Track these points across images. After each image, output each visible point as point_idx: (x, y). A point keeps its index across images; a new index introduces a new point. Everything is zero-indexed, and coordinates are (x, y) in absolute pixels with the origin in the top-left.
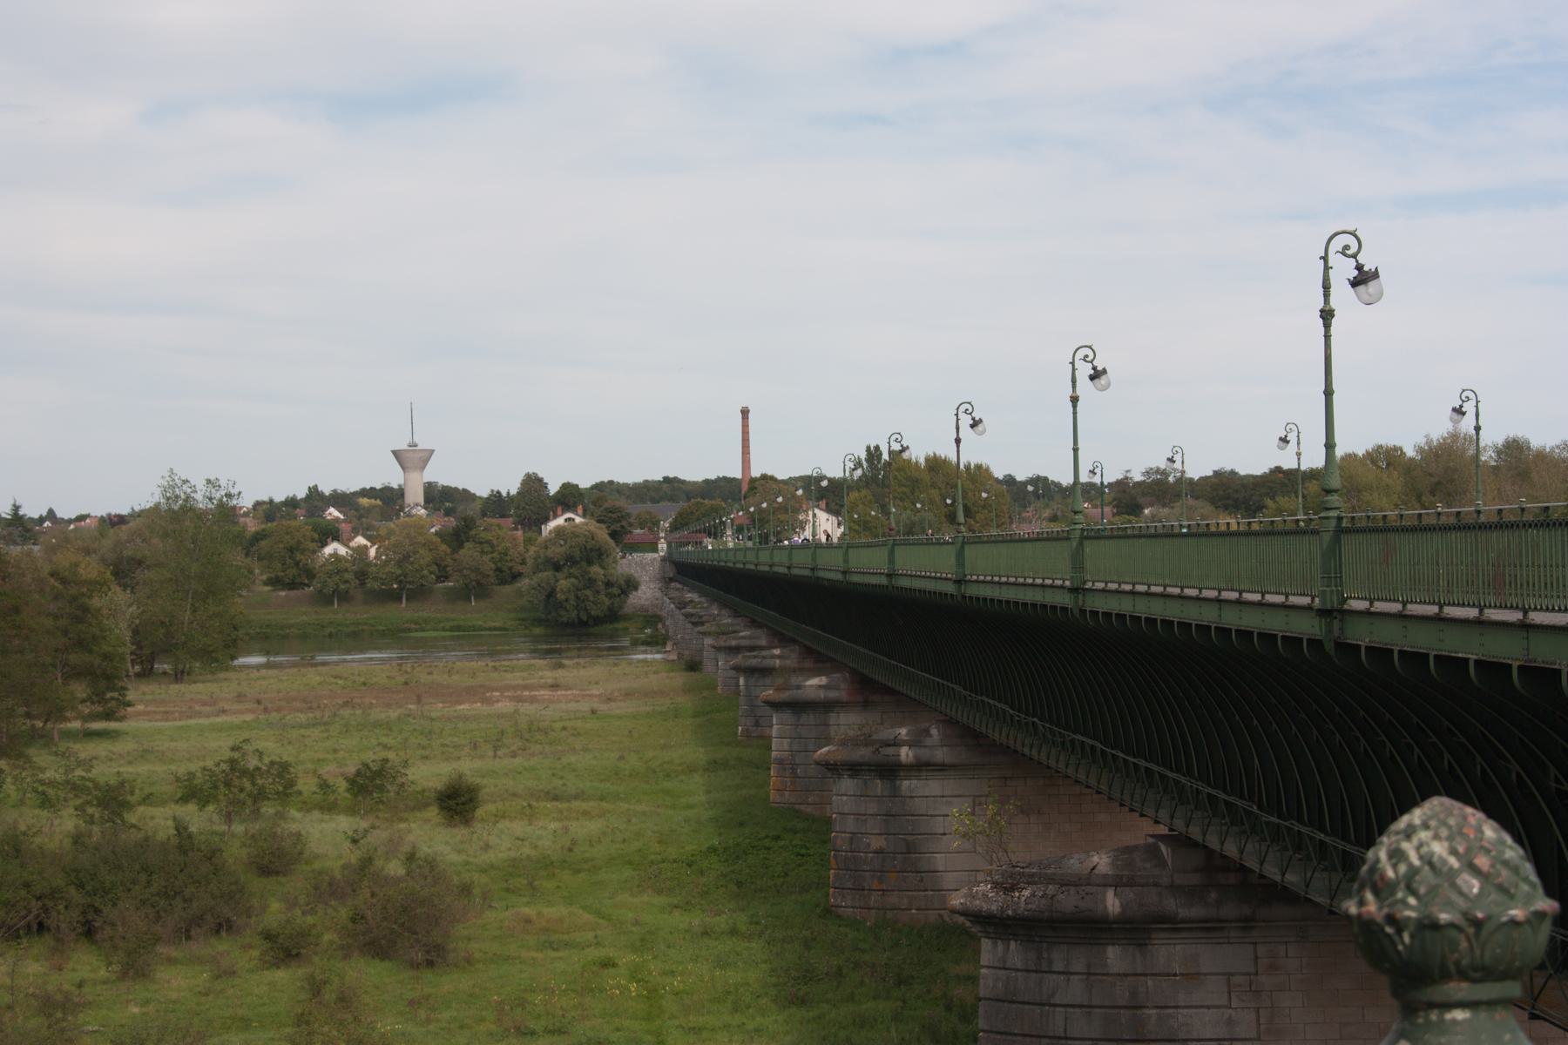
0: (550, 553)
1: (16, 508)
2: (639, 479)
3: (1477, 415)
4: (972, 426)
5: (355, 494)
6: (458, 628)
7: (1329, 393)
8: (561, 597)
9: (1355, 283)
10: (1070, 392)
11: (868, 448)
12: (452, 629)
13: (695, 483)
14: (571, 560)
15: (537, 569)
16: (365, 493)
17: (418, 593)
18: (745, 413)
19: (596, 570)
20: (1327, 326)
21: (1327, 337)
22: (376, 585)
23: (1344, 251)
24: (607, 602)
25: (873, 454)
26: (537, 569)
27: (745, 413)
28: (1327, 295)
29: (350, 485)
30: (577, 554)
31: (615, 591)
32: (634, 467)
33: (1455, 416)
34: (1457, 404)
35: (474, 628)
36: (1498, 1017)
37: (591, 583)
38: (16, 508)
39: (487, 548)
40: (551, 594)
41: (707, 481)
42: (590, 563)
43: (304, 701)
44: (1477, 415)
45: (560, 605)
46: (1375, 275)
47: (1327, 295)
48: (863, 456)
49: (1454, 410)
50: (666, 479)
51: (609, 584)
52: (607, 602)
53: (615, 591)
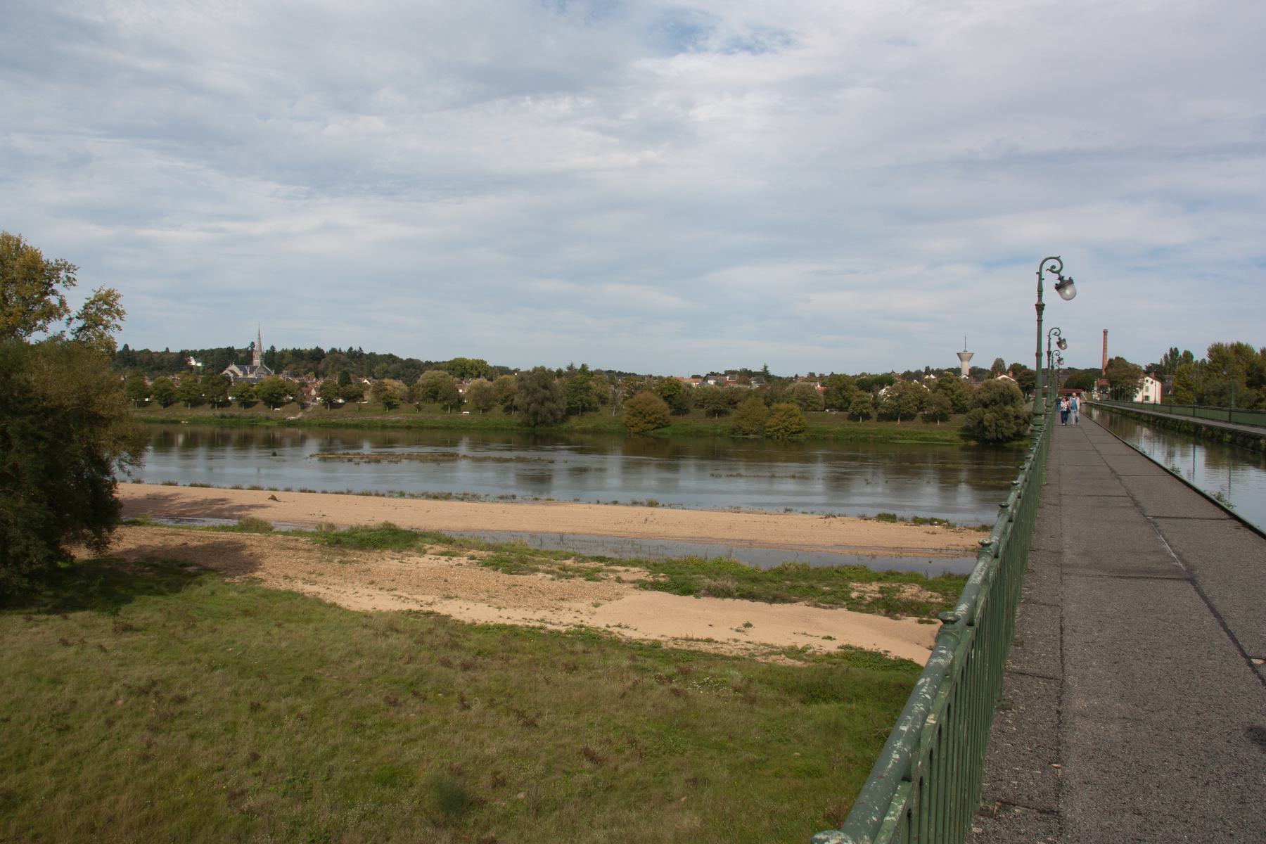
0: (981, 396)
4: (1058, 287)
6: (924, 439)
8: (986, 423)
9: (1058, 287)
10: (1036, 301)
12: (921, 439)
14: (994, 402)
15: (974, 406)
16: (949, 370)
17: (908, 417)
18: (1105, 332)
19: (1009, 408)
21: (1040, 321)
22: (884, 411)
23: (1052, 269)
24: (1015, 428)
25: (1174, 352)
26: (974, 406)
27: (1105, 332)
28: (1040, 296)
30: (998, 398)
31: (1021, 421)
32: (877, 369)
35: (934, 439)
37: (1006, 416)
39: (949, 392)
40: (981, 422)
41: (147, 352)
42: (1006, 404)
45: (985, 428)
46: (1071, 281)
47: (1040, 296)
51: (1017, 417)
52: (1015, 428)
53: (1021, 421)
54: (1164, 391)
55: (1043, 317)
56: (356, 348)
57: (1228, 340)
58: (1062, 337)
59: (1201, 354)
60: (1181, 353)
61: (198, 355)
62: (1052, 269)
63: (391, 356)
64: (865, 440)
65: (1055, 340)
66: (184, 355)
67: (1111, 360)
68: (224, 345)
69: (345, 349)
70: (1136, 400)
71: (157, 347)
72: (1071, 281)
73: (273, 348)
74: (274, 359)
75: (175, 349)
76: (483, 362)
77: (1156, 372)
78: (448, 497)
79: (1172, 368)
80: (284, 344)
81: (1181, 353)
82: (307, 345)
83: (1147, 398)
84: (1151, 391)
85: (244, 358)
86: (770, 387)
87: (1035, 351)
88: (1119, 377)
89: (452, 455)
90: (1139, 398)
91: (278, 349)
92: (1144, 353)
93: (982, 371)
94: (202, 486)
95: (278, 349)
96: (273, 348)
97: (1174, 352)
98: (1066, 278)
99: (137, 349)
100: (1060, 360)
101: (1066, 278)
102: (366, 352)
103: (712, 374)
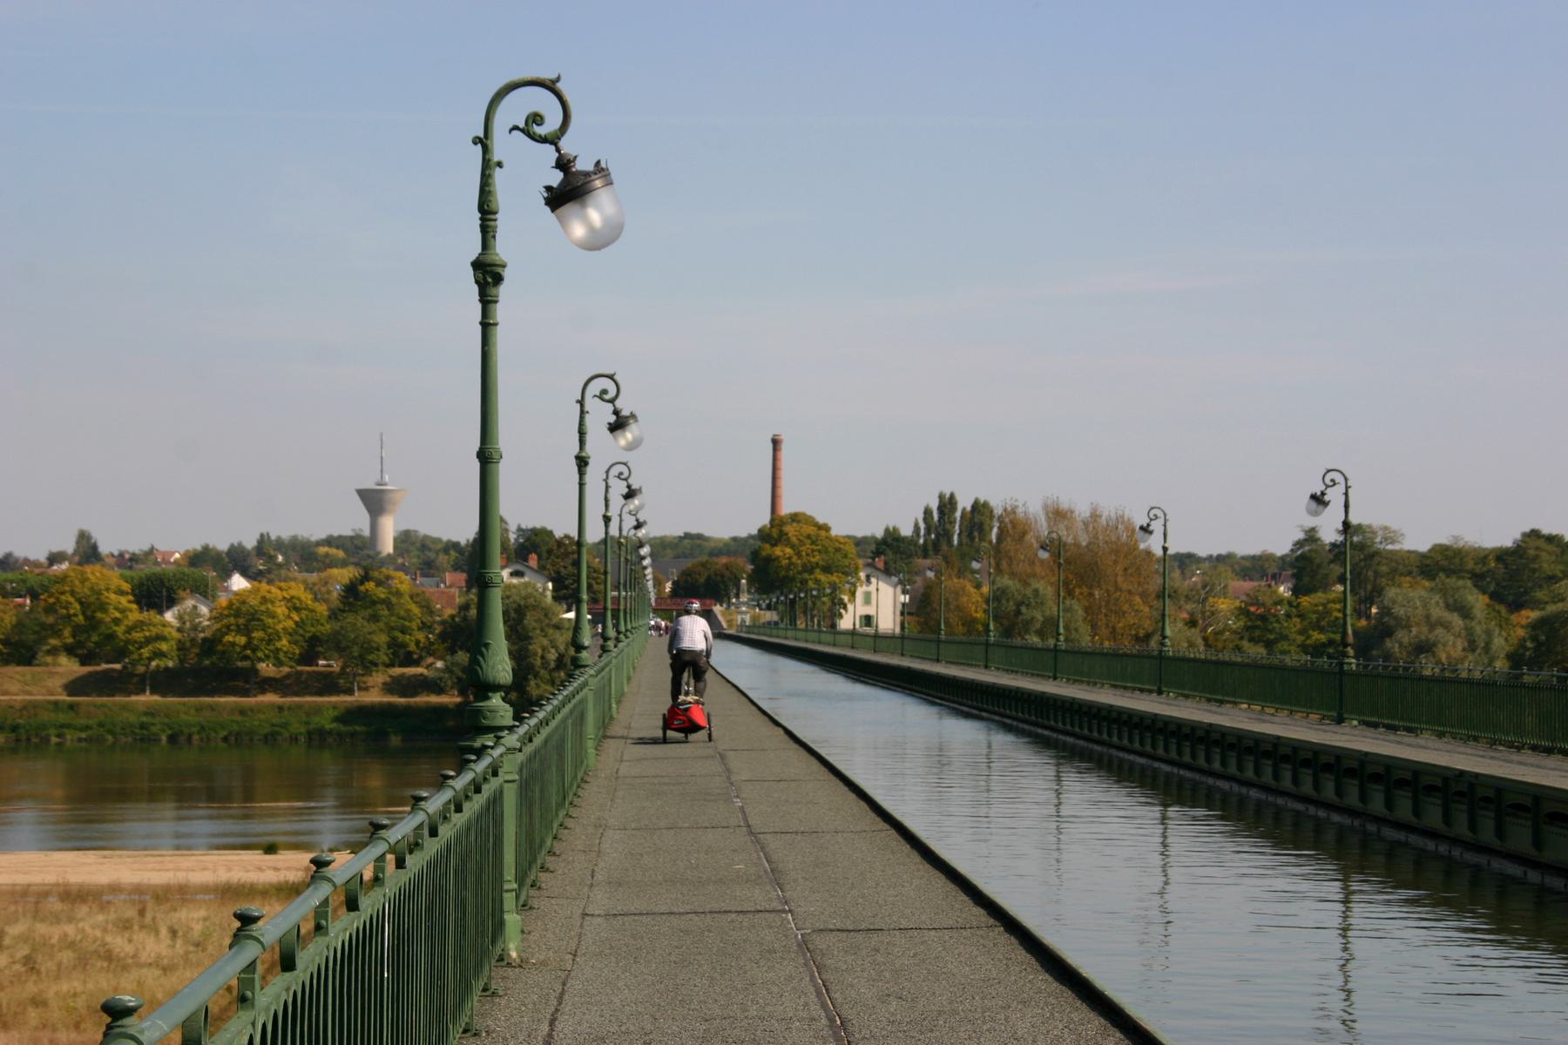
3: (1347, 506)
5: (318, 544)
7: (486, 458)
10: (505, 293)
11: (941, 497)
13: (720, 540)
16: (329, 541)
18: (776, 443)
21: (487, 326)
23: (530, 127)
25: (947, 504)
27: (776, 443)
32: (174, 539)
33: (1314, 505)
34: (1318, 491)
41: (735, 539)
44: (1347, 506)
47: (487, 231)
48: (934, 505)
49: (1313, 497)
50: (687, 536)
55: (501, 312)
58: (582, 149)
59: (273, 537)
60: (1103, 521)
62: (619, 476)
64: (270, 739)
65: (619, 488)
72: (1326, 504)
76: (551, 532)
77: (889, 553)
84: (879, 604)
87: (476, 444)
88: (780, 576)
100: (639, 526)
101: (1326, 498)
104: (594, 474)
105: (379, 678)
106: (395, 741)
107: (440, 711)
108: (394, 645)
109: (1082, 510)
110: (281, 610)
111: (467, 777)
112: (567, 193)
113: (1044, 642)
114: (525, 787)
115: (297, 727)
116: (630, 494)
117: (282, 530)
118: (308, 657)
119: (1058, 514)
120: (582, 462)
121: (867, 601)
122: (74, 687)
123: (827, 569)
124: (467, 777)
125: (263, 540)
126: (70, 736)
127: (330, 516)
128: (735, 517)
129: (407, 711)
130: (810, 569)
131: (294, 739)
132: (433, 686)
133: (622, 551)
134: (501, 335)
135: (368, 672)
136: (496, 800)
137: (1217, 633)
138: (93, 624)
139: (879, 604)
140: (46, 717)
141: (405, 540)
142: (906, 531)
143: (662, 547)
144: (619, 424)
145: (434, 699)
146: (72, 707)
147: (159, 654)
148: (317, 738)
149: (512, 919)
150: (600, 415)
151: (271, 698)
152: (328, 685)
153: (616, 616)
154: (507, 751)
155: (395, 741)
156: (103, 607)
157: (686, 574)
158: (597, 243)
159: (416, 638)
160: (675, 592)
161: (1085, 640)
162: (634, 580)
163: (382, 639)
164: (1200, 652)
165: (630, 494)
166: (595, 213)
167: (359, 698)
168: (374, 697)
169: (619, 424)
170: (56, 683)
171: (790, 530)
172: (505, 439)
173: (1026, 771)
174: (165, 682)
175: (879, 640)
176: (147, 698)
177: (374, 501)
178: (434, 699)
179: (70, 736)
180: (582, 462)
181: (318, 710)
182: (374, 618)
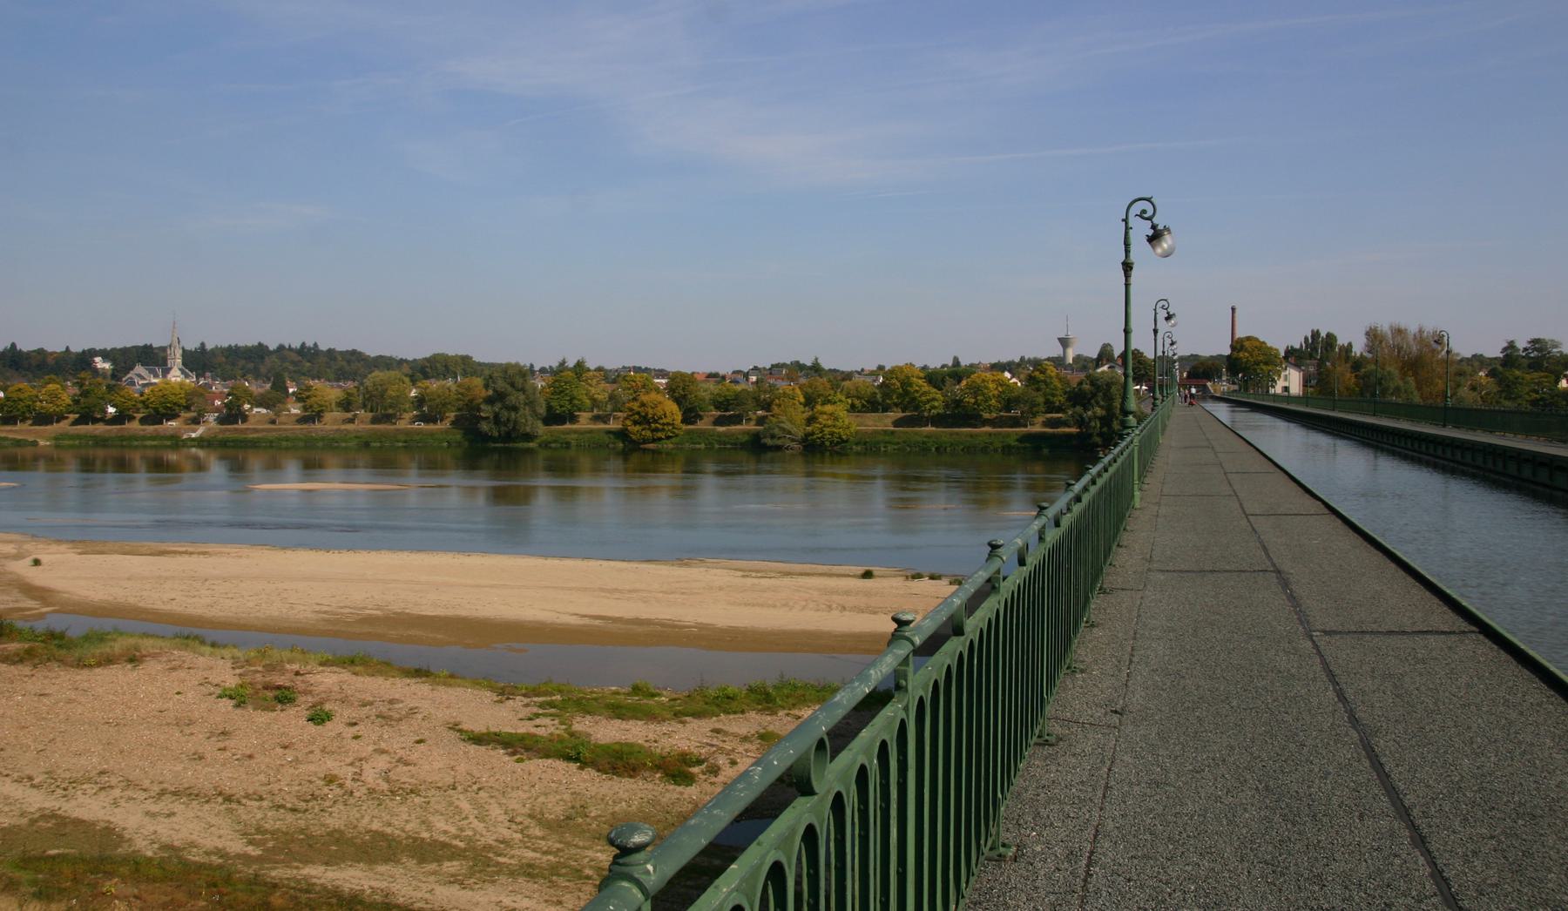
1: (13, 345)
2: (504, 361)
10: (1134, 273)
18: (1233, 309)
20: (1127, 276)
21: (1127, 285)
23: (1142, 215)
25: (1315, 334)
27: (1233, 309)
28: (1127, 251)
29: (612, 364)
36: (1414, 591)
38: (13, 345)
41: (41, 352)
43: (280, 448)
47: (1127, 251)
54: (1306, 382)
55: (1133, 280)
56: (310, 344)
57: (1384, 325)
60: (1323, 334)
61: (106, 355)
62: (1142, 215)
63: (354, 352)
64: (984, 450)
65: (1168, 341)
66: (93, 353)
67: (1241, 340)
68: (140, 342)
69: (296, 345)
70: (1272, 391)
71: (55, 345)
73: (203, 344)
74: (197, 361)
75: (77, 348)
77: (1294, 356)
78: (284, 527)
79: (1317, 353)
80: (217, 338)
81: (1323, 334)
82: (247, 340)
83: (1286, 389)
84: (1291, 381)
85: (152, 357)
86: (815, 381)
88: (1245, 366)
89: (573, 488)
90: (1278, 389)
91: (209, 347)
92: (1283, 335)
93: (1087, 360)
94: (299, 527)
95: (209, 347)
96: (203, 344)
97: (1315, 334)
98: (1160, 227)
99: (25, 349)
102: (323, 347)
103: (756, 368)
104: (1160, 335)
105: (1040, 419)
106: (1046, 451)
107: (1069, 436)
108: (1047, 402)
109: (1413, 328)
110: (991, 386)
111: (1110, 457)
112: (1155, 237)
113: (1380, 397)
114: (1140, 453)
115: (998, 445)
116: (1172, 344)
117: (1029, 355)
118: (1008, 408)
119: (1399, 332)
120: (1156, 331)
121: (1286, 379)
122: (897, 423)
123: (1266, 364)
124: (1110, 457)
125: (1022, 359)
126: (890, 448)
127: (1047, 349)
128: (1217, 345)
129: (1054, 436)
130: (1257, 363)
131: (996, 450)
132: (1065, 424)
133: (1166, 362)
134: (1132, 289)
135: (1034, 415)
136: (1131, 455)
137: (549, 408)
138: (906, 393)
139: (1291, 381)
140: (881, 438)
141: (1077, 358)
142: (1297, 346)
143: (1182, 359)
144: (1168, 318)
145: (1067, 430)
146: (893, 433)
147: (934, 407)
148: (1007, 450)
149: (1137, 493)
150: (1162, 314)
151: (987, 429)
152: (1016, 422)
153: (1161, 387)
154: (1135, 437)
155: (1046, 451)
156: (910, 385)
157: (1194, 368)
158: (1166, 255)
159: (1059, 399)
160: (1189, 376)
161: (1417, 399)
162: (1169, 372)
163: (1041, 400)
164: (1479, 405)
165: (1172, 344)
166: (1166, 244)
167: (1030, 429)
168: (1037, 429)
169: (1168, 318)
170: (889, 421)
171: (1247, 344)
172: (1133, 325)
173: (1396, 475)
174: (938, 421)
175: (1290, 399)
176: (930, 428)
177: (1064, 342)
178: (1067, 430)
179: (890, 448)
180: (1156, 331)
181: (1008, 435)
182: (1038, 390)
